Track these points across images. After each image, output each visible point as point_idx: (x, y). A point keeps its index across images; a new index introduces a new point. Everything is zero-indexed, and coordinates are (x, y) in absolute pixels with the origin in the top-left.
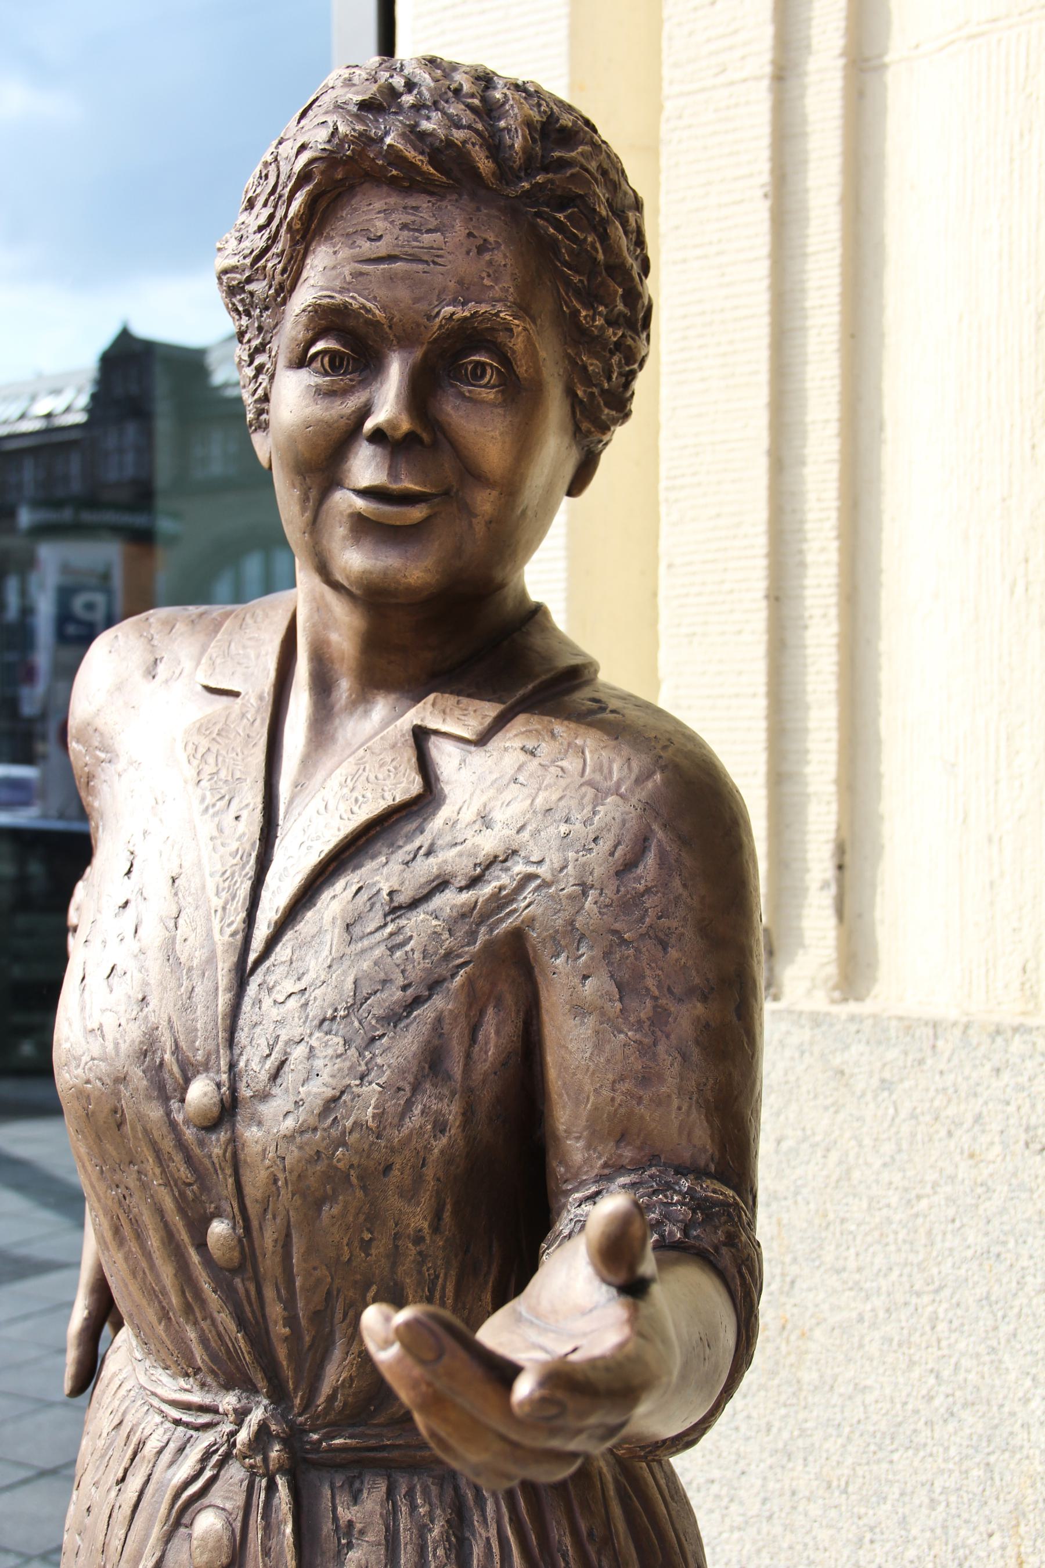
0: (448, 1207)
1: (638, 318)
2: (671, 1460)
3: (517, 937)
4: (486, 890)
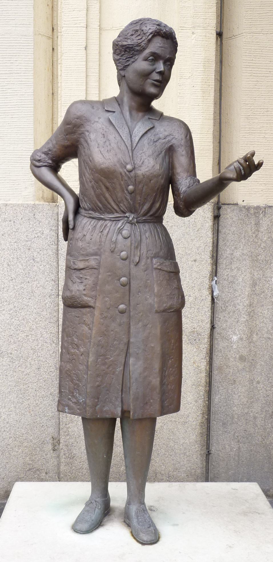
1: (177, 44)
4: (167, 139)
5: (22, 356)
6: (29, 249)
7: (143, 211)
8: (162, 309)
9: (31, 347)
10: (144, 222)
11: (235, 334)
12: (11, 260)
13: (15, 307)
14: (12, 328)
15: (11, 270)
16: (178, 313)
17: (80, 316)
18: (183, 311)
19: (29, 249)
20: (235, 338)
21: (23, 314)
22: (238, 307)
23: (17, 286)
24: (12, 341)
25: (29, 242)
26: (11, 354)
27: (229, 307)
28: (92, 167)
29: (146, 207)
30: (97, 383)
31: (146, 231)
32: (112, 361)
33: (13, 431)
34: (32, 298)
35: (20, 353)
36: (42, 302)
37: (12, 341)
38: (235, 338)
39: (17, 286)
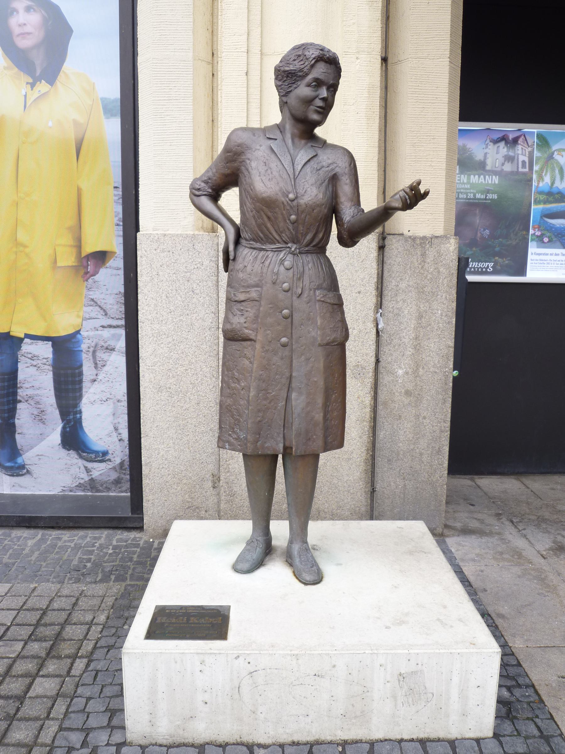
1: (341, 69)
5: (181, 391)
6: (188, 281)
8: (325, 342)
11: (400, 368)
13: (173, 340)
15: (169, 302)
16: (342, 346)
18: (347, 344)
19: (188, 281)
20: (401, 372)
22: (404, 340)
23: (176, 319)
24: (171, 375)
26: (170, 388)
27: (394, 341)
28: (253, 196)
29: (309, 237)
30: (259, 419)
35: (179, 388)
37: (171, 375)
38: (400, 372)
39: (176, 319)
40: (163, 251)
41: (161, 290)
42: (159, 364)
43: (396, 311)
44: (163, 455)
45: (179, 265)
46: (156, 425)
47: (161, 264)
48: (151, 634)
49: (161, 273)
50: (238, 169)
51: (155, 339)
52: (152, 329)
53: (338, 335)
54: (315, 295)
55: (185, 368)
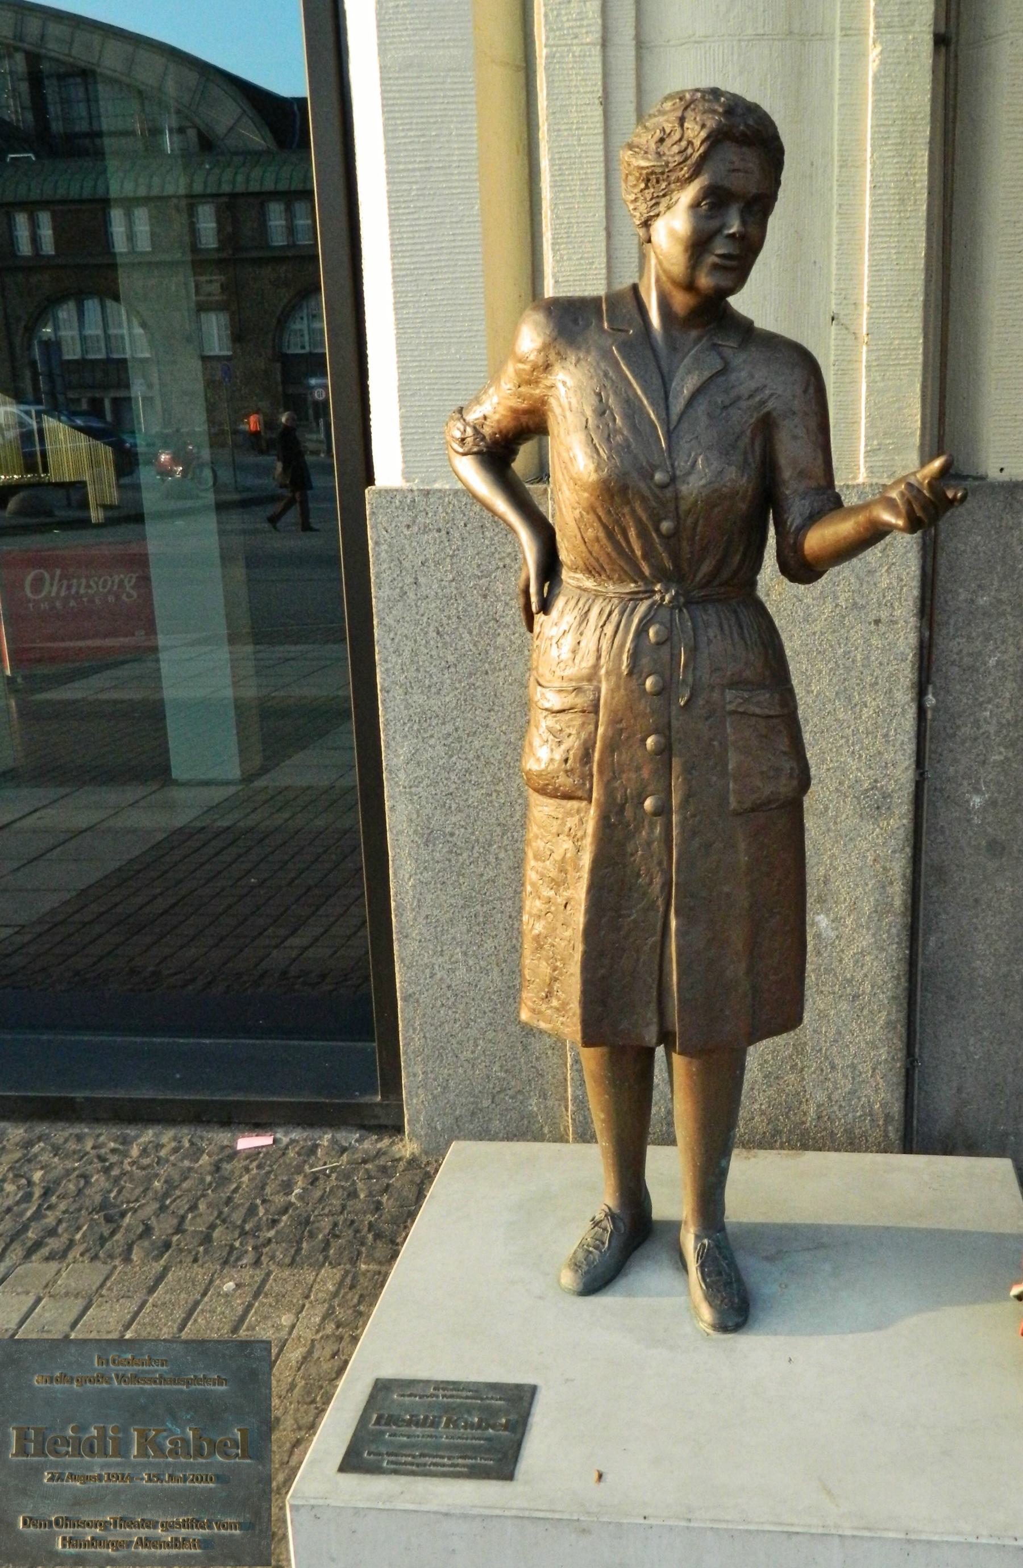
0: (70, 665)
1: (781, 151)
2: (546, 296)
3: (768, 414)
4: (757, 399)
5: (477, 841)
6: (485, 596)
7: (700, 575)
8: (748, 805)
9: (497, 819)
10: (704, 601)
11: (977, 791)
12: (445, 621)
13: (456, 730)
14: (453, 777)
15: (445, 644)
16: (792, 811)
17: (560, 816)
18: (807, 801)
19: (485, 596)
20: (978, 800)
21: (477, 744)
22: (985, 727)
23: (460, 682)
24: (454, 806)
25: (483, 581)
26: (452, 835)
27: (963, 730)
28: (575, 476)
29: (706, 568)
30: (602, 972)
31: (707, 625)
32: (635, 921)
33: (461, 1007)
34: (496, 708)
35: (473, 833)
36: (519, 719)
37: (454, 806)
38: (977, 801)
39: (460, 682)
40: (425, 530)
41: (425, 620)
42: (426, 782)
43: (967, 661)
44: (441, 979)
45: (463, 561)
46: (424, 915)
47: (422, 558)
48: (355, 1461)
49: (422, 580)
50: (543, 402)
51: (415, 727)
52: (408, 706)
53: (785, 787)
54: (724, 698)
55: (484, 791)
